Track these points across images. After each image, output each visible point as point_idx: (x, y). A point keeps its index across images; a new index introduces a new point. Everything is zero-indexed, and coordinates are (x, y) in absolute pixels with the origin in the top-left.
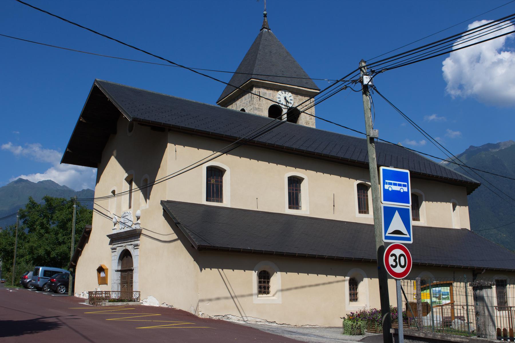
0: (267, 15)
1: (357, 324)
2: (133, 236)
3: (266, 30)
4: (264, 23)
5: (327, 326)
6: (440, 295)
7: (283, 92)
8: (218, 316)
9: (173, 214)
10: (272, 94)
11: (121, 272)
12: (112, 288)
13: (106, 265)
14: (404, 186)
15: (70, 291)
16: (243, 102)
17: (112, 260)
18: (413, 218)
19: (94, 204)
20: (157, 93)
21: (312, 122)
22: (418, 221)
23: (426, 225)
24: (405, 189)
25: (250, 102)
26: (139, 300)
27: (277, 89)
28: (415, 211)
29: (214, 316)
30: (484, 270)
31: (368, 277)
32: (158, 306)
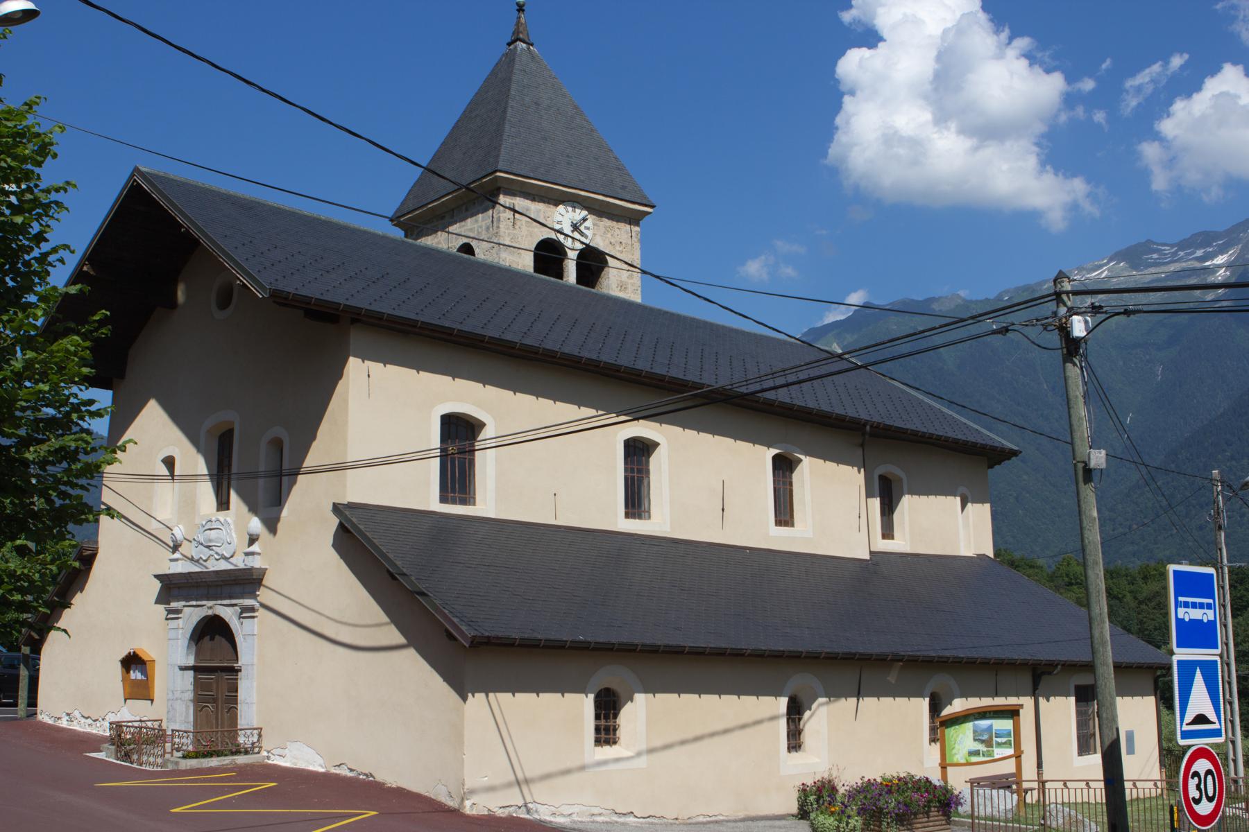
0: (524, 8)
1: (848, 824)
2: (237, 584)
3: (524, 45)
4: (518, 28)
5: (741, 815)
6: (991, 738)
7: (570, 209)
8: (508, 806)
9: (377, 544)
10: (542, 212)
11: (195, 671)
12: (168, 712)
13: (148, 650)
14: (1209, 606)
15: (23, 705)
16: (469, 228)
17: (170, 639)
18: (777, 487)
19: (104, 487)
20: (291, 210)
21: (633, 285)
22: (889, 539)
23: (907, 549)
24: (1208, 615)
25: (488, 228)
26: (256, 750)
27: (555, 200)
28: (781, 472)
29: (497, 808)
30: (1059, 667)
31: (646, 691)
32: (322, 770)
